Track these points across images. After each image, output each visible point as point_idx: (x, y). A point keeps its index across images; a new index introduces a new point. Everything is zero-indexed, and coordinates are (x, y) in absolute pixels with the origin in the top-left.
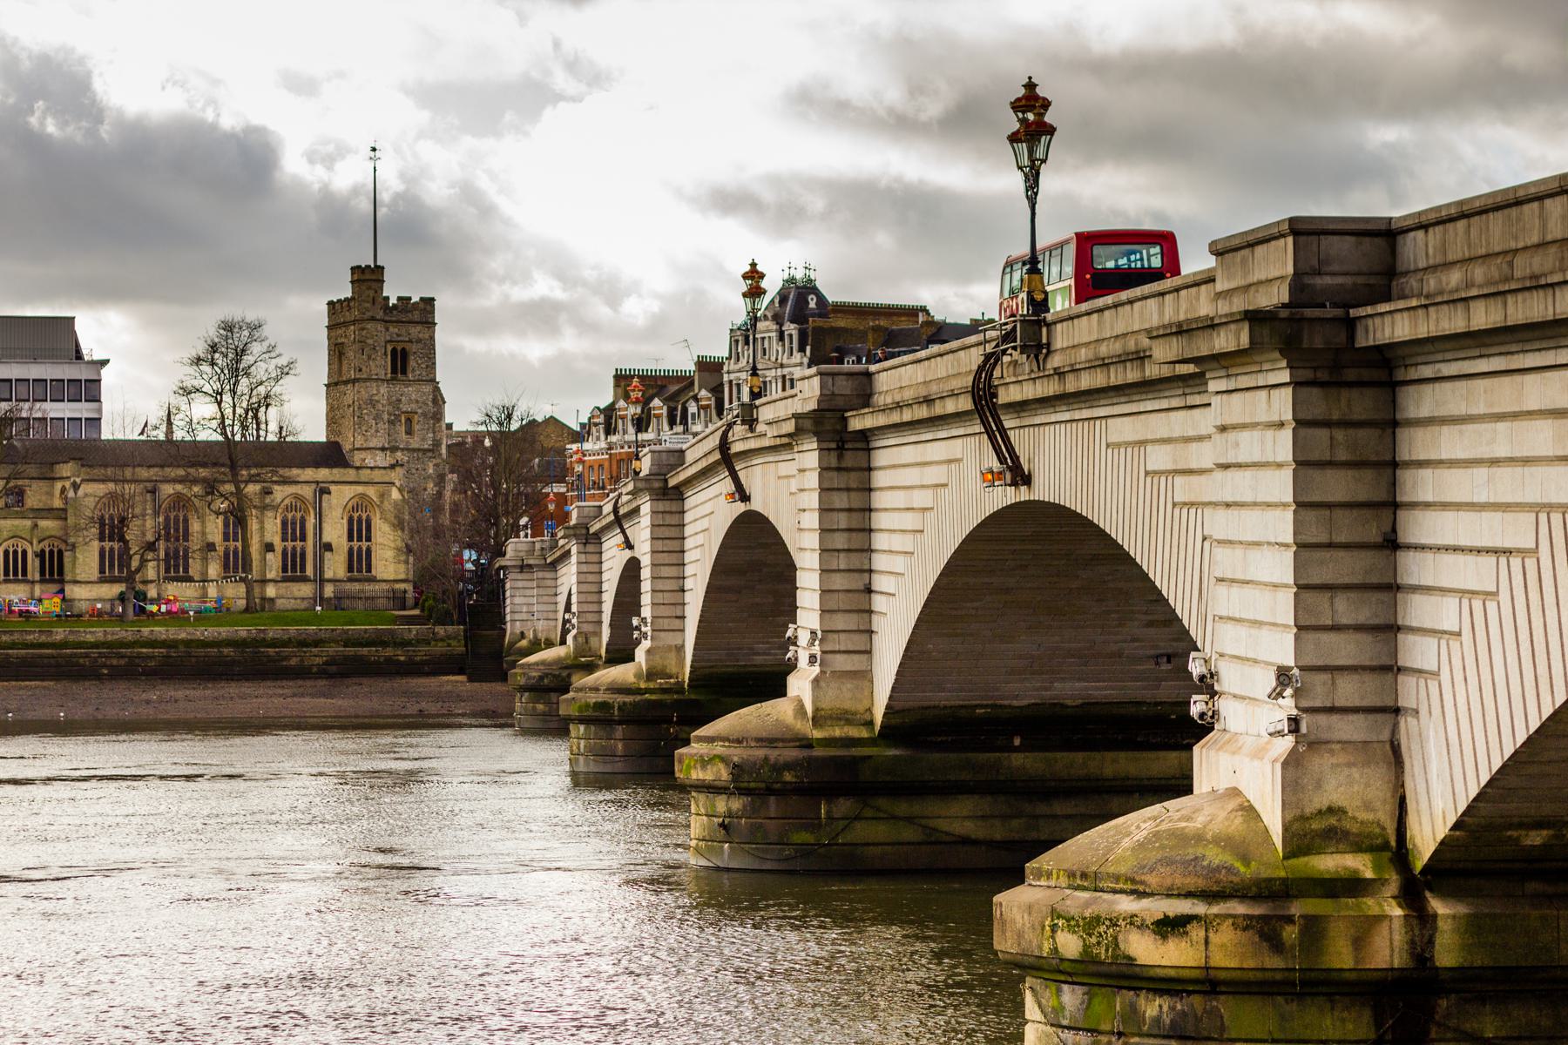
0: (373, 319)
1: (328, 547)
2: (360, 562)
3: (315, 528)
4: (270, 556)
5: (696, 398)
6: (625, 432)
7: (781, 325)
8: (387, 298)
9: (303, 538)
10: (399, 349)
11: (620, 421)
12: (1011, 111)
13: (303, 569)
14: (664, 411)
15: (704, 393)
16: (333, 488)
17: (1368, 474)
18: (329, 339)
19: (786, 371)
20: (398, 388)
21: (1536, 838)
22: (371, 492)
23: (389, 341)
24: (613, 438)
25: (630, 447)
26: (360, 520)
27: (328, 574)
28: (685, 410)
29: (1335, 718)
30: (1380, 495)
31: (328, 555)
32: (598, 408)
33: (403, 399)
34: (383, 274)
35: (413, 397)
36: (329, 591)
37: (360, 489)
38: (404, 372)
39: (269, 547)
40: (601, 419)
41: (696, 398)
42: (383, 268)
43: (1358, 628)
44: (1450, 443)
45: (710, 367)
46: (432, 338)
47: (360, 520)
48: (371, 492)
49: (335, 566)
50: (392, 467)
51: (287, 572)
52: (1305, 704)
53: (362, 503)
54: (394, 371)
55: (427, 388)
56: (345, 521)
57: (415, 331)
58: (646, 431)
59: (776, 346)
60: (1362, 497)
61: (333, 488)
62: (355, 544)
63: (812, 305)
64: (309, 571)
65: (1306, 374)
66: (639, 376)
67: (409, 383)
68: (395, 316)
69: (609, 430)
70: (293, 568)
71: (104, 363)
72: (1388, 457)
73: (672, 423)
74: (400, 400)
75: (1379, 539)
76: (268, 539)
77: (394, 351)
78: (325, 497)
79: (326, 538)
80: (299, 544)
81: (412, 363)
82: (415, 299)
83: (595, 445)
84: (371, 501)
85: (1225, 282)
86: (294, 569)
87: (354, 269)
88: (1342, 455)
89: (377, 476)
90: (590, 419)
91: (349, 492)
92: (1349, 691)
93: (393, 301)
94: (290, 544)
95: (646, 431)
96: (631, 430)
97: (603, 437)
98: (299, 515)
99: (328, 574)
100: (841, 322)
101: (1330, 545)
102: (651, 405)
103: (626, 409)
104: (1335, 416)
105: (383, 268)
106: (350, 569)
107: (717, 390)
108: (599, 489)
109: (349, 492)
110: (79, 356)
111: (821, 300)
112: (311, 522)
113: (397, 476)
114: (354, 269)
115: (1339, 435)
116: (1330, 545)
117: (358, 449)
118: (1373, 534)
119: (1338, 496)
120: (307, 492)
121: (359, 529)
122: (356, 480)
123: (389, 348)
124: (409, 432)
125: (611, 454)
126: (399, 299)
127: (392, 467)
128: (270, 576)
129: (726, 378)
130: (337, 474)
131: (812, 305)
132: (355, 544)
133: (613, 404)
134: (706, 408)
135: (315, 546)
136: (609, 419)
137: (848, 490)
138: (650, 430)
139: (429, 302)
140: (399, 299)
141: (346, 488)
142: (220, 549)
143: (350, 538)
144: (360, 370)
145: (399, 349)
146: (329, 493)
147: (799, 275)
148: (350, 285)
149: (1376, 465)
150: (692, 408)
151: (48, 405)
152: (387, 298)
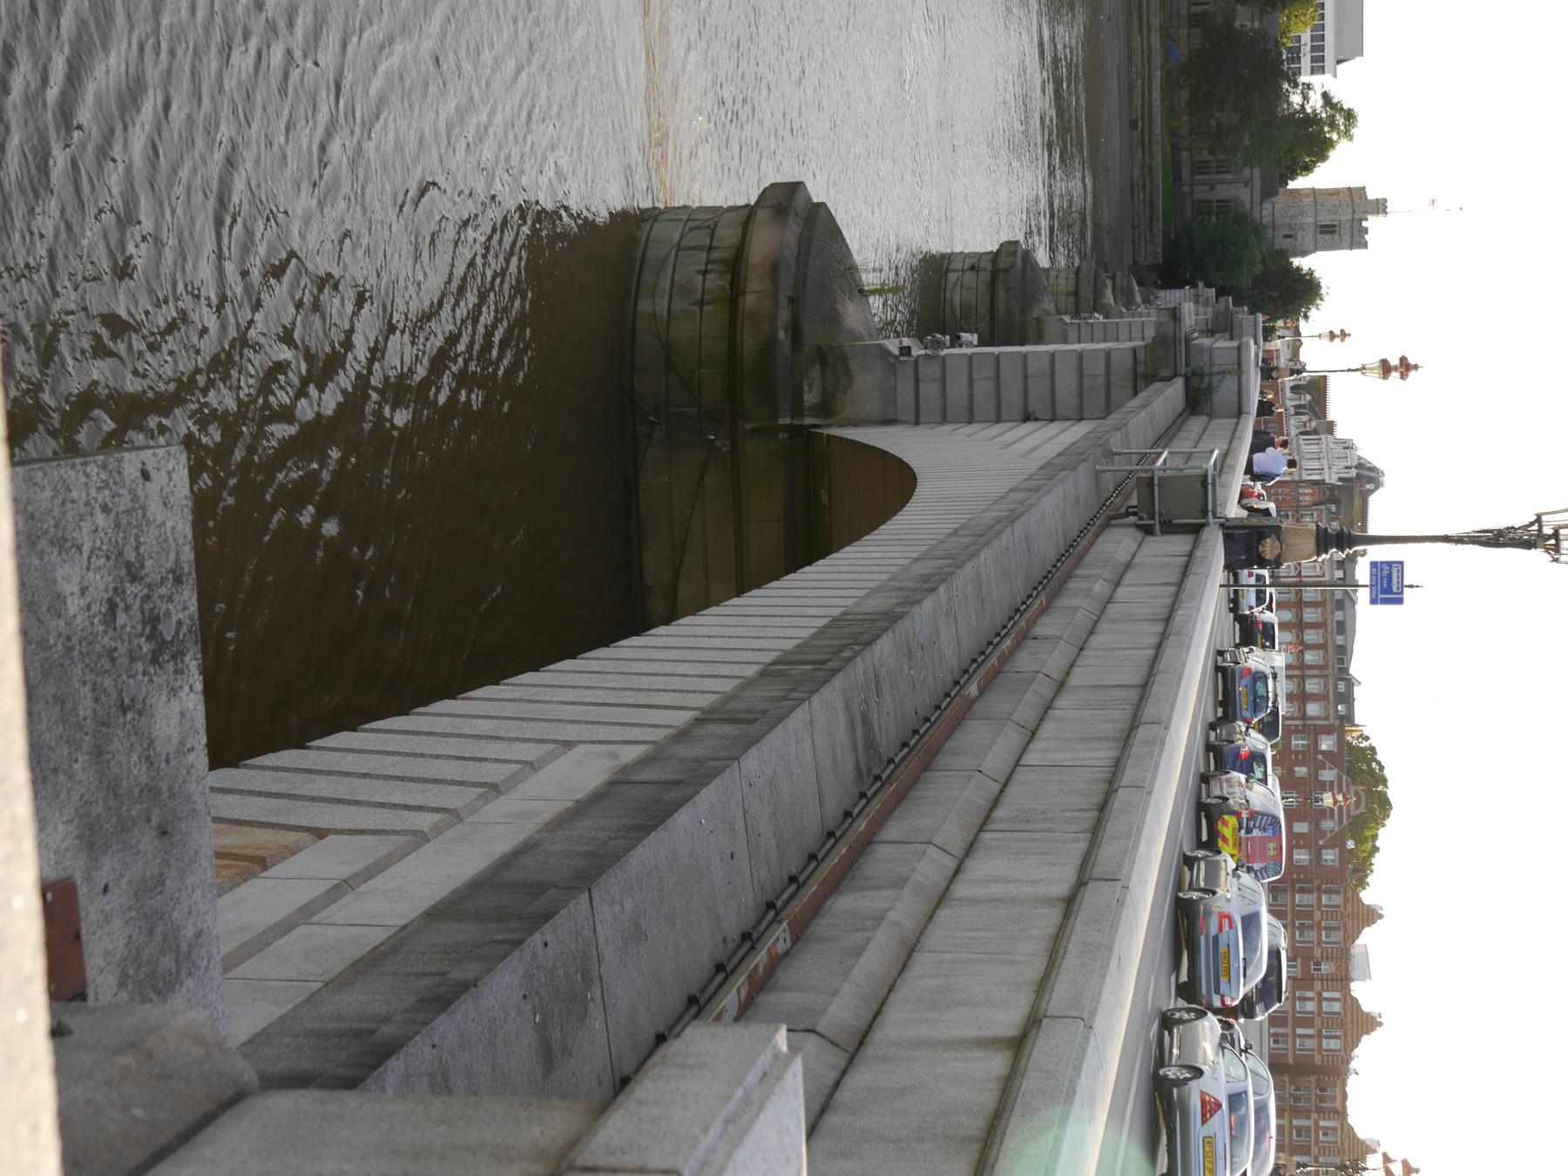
0: (1354, 212)
1: (1212, 187)
5: (1310, 420)
7: (1356, 467)
9: (1218, 173)
12: (1355, 252)
13: (1199, 173)
14: (1303, 402)
15: (1314, 424)
16: (1248, 190)
17: (1074, 401)
19: (1326, 470)
20: (1311, 230)
21: (825, 498)
27: (1196, 189)
28: (1303, 414)
29: (912, 382)
30: (1060, 411)
31: (1207, 188)
36: (1186, 189)
38: (1321, 232)
41: (1310, 420)
43: (971, 397)
44: (1160, 610)
45: (1330, 427)
46: (1342, 248)
52: (921, 361)
54: (1322, 226)
55: (1311, 247)
57: (1347, 238)
59: (1342, 464)
60: (1058, 397)
61: (1248, 190)
62: (1215, 204)
63: (1368, 486)
64: (1198, 177)
65: (1141, 356)
67: (1315, 234)
71: (1335, 76)
72: (1086, 415)
73: (1296, 407)
75: (1030, 410)
79: (1218, 186)
81: (1327, 237)
87: (1385, 200)
88: (1087, 383)
92: (930, 390)
93: (1364, 224)
99: (1196, 189)
100: (1357, 502)
101: (1026, 377)
104: (1113, 378)
107: (1315, 432)
110: (1339, 62)
111: (1371, 492)
114: (1385, 200)
115: (1101, 381)
116: (1026, 377)
118: (1034, 406)
119: (1058, 382)
124: (1286, 236)
129: (1323, 436)
130: (1257, 192)
131: (1368, 486)
134: (1305, 425)
139: (1365, 246)
143: (1218, 201)
149: (1081, 408)
150: (1305, 418)
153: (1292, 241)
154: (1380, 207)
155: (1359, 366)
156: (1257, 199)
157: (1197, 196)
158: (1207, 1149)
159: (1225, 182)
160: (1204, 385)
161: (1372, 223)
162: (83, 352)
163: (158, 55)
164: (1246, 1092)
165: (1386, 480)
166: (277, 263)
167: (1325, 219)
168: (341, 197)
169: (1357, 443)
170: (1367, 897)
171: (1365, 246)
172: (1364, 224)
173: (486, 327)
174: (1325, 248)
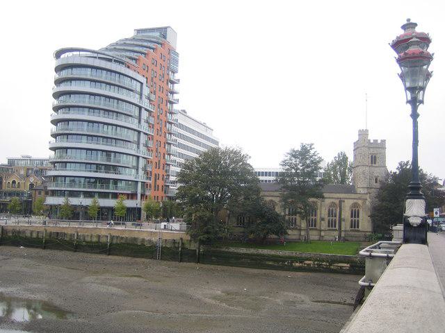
2: (354, 225)
9: (336, 216)
16: (346, 200)
38: (375, 163)
46: (385, 153)
48: (360, 202)
49: (346, 226)
50: (367, 194)
53: (355, 205)
54: (372, 163)
61: (346, 200)
66: (258, 198)
68: (372, 146)
70: (331, 224)
76: (323, 216)
80: (334, 218)
85: (178, 170)
91: (351, 202)
93: (372, 141)
94: (353, 219)
106: (352, 227)
120: (337, 202)
121: (355, 214)
123: (370, 156)
124: (376, 182)
127: (367, 194)
128: (322, 229)
139: (383, 141)
143: (352, 217)
147: (242, 153)
152: (370, 140)
155: (409, 107)
156: (353, 196)
157: (348, 228)
158: (82, 180)
160: (377, 200)
161: (371, 137)
165: (431, 36)
167: (368, 161)
169: (180, 56)
171: (383, 141)
172: (372, 141)
174: (384, 161)
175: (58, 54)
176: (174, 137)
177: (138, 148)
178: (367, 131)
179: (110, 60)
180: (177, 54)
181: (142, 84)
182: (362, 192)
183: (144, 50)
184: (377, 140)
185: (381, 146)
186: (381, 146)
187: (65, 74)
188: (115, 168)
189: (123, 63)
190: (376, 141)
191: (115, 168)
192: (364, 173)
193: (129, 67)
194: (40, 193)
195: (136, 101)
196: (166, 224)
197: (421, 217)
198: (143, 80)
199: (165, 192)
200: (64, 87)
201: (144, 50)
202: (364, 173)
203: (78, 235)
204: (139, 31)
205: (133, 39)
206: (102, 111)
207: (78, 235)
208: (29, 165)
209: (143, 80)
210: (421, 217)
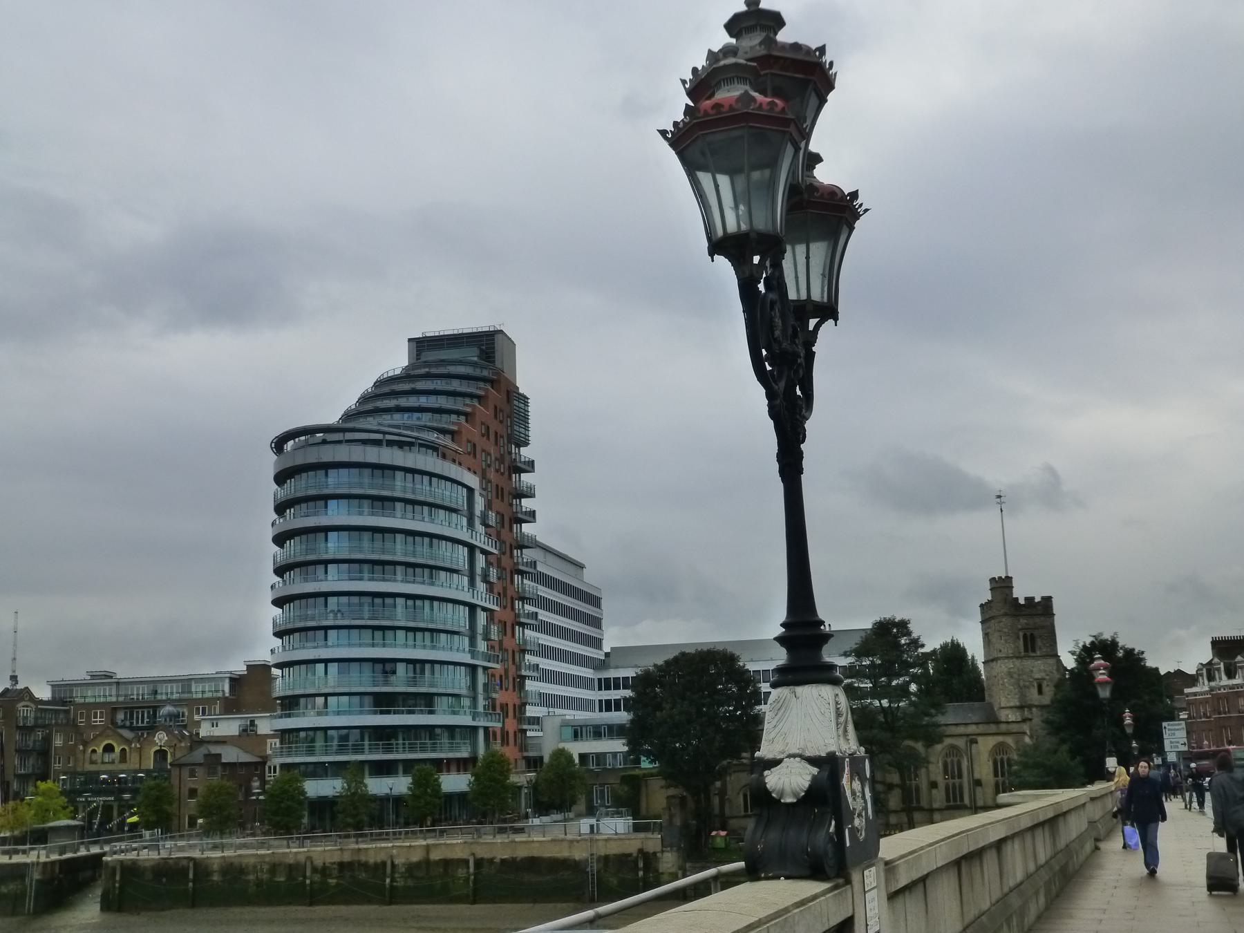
1: (978, 783)
3: (968, 769)
4: (934, 791)
6: (1220, 679)
8: (1017, 599)
9: (960, 776)
10: (1028, 634)
11: (1216, 672)
16: (980, 739)
18: (982, 630)
20: (1028, 663)
22: (1009, 740)
23: (1021, 629)
24: (1213, 684)
25: (1224, 689)
26: (1002, 760)
31: (979, 789)
32: (1201, 664)
33: (1034, 669)
34: (1011, 582)
35: (1042, 668)
37: (1000, 739)
39: (934, 785)
40: (1204, 671)
42: (1011, 578)
47: (1002, 760)
48: (1009, 740)
51: (748, 811)
54: (1026, 650)
56: (991, 763)
57: (1039, 621)
58: (1235, 678)
64: (967, 801)
69: (1211, 678)
74: (1032, 671)
76: (933, 778)
77: (1025, 637)
78: (974, 746)
79: (977, 776)
80: (957, 781)
82: (1038, 599)
83: (1203, 687)
84: (1009, 746)
86: (955, 800)
89: (1014, 728)
90: (1197, 671)
91: (991, 742)
95: (1235, 678)
96: (1224, 677)
97: (1206, 682)
98: (955, 759)
102: (1236, 660)
103: (1219, 664)
105: (1011, 578)
106: (948, 800)
108: (1207, 717)
109: (991, 742)
112: (965, 764)
113: (1026, 727)
117: (1003, 708)
120: (961, 743)
122: (998, 732)
123: (1021, 634)
124: (1040, 692)
125: (1212, 695)
126: (1026, 599)
128: (936, 805)
132: (951, 781)
133: (1212, 660)
135: (969, 782)
136: (1209, 670)
137: (1008, 723)
138: (1237, 677)
140: (1026, 599)
141: (990, 738)
142: (942, 786)
143: (996, 775)
144: (1000, 651)
145: (1028, 634)
146: (977, 743)
148: (990, 591)
151: (556, 710)
152: (1017, 599)
153: (1044, 684)
154: (1002, 586)
159: (971, 770)
161: (1020, 592)
162: (860, 815)
163: (433, 610)
164: (431, 712)
166: (1065, 747)
168: (202, 856)
170: (813, 147)
171: (1047, 600)
172: (1022, 601)
173: (534, 564)
174: (1052, 610)
175: (279, 444)
176: (529, 608)
177: (473, 642)
178: (1009, 579)
179: (377, 443)
180: (524, 399)
181: (470, 490)
182: (1012, 718)
183: (459, 404)
184: (1033, 598)
185: (1042, 609)
186: (1042, 609)
187: (294, 488)
188: (427, 701)
189: (411, 444)
190: (1030, 600)
191: (427, 701)
192: (1010, 674)
193: (444, 457)
194: (192, 774)
195: (464, 535)
196: (593, 821)
197: (813, 761)
198: (473, 481)
199: (521, 750)
200: (295, 520)
201: (459, 404)
202: (1010, 674)
203: (392, 863)
204: (421, 345)
205: (406, 376)
206: (366, 567)
207: (392, 863)
208: (110, 695)
209: (473, 481)
210: (813, 761)
